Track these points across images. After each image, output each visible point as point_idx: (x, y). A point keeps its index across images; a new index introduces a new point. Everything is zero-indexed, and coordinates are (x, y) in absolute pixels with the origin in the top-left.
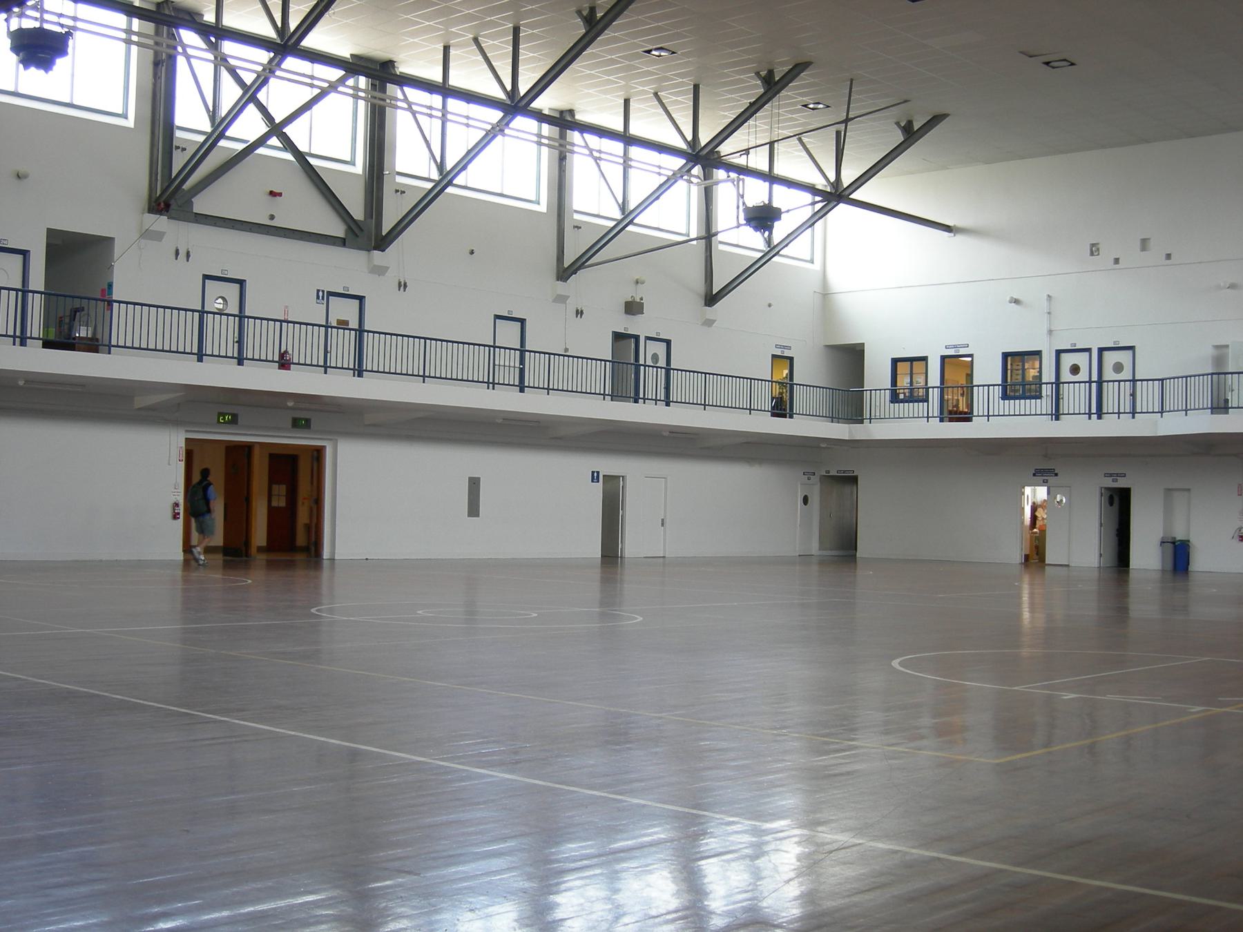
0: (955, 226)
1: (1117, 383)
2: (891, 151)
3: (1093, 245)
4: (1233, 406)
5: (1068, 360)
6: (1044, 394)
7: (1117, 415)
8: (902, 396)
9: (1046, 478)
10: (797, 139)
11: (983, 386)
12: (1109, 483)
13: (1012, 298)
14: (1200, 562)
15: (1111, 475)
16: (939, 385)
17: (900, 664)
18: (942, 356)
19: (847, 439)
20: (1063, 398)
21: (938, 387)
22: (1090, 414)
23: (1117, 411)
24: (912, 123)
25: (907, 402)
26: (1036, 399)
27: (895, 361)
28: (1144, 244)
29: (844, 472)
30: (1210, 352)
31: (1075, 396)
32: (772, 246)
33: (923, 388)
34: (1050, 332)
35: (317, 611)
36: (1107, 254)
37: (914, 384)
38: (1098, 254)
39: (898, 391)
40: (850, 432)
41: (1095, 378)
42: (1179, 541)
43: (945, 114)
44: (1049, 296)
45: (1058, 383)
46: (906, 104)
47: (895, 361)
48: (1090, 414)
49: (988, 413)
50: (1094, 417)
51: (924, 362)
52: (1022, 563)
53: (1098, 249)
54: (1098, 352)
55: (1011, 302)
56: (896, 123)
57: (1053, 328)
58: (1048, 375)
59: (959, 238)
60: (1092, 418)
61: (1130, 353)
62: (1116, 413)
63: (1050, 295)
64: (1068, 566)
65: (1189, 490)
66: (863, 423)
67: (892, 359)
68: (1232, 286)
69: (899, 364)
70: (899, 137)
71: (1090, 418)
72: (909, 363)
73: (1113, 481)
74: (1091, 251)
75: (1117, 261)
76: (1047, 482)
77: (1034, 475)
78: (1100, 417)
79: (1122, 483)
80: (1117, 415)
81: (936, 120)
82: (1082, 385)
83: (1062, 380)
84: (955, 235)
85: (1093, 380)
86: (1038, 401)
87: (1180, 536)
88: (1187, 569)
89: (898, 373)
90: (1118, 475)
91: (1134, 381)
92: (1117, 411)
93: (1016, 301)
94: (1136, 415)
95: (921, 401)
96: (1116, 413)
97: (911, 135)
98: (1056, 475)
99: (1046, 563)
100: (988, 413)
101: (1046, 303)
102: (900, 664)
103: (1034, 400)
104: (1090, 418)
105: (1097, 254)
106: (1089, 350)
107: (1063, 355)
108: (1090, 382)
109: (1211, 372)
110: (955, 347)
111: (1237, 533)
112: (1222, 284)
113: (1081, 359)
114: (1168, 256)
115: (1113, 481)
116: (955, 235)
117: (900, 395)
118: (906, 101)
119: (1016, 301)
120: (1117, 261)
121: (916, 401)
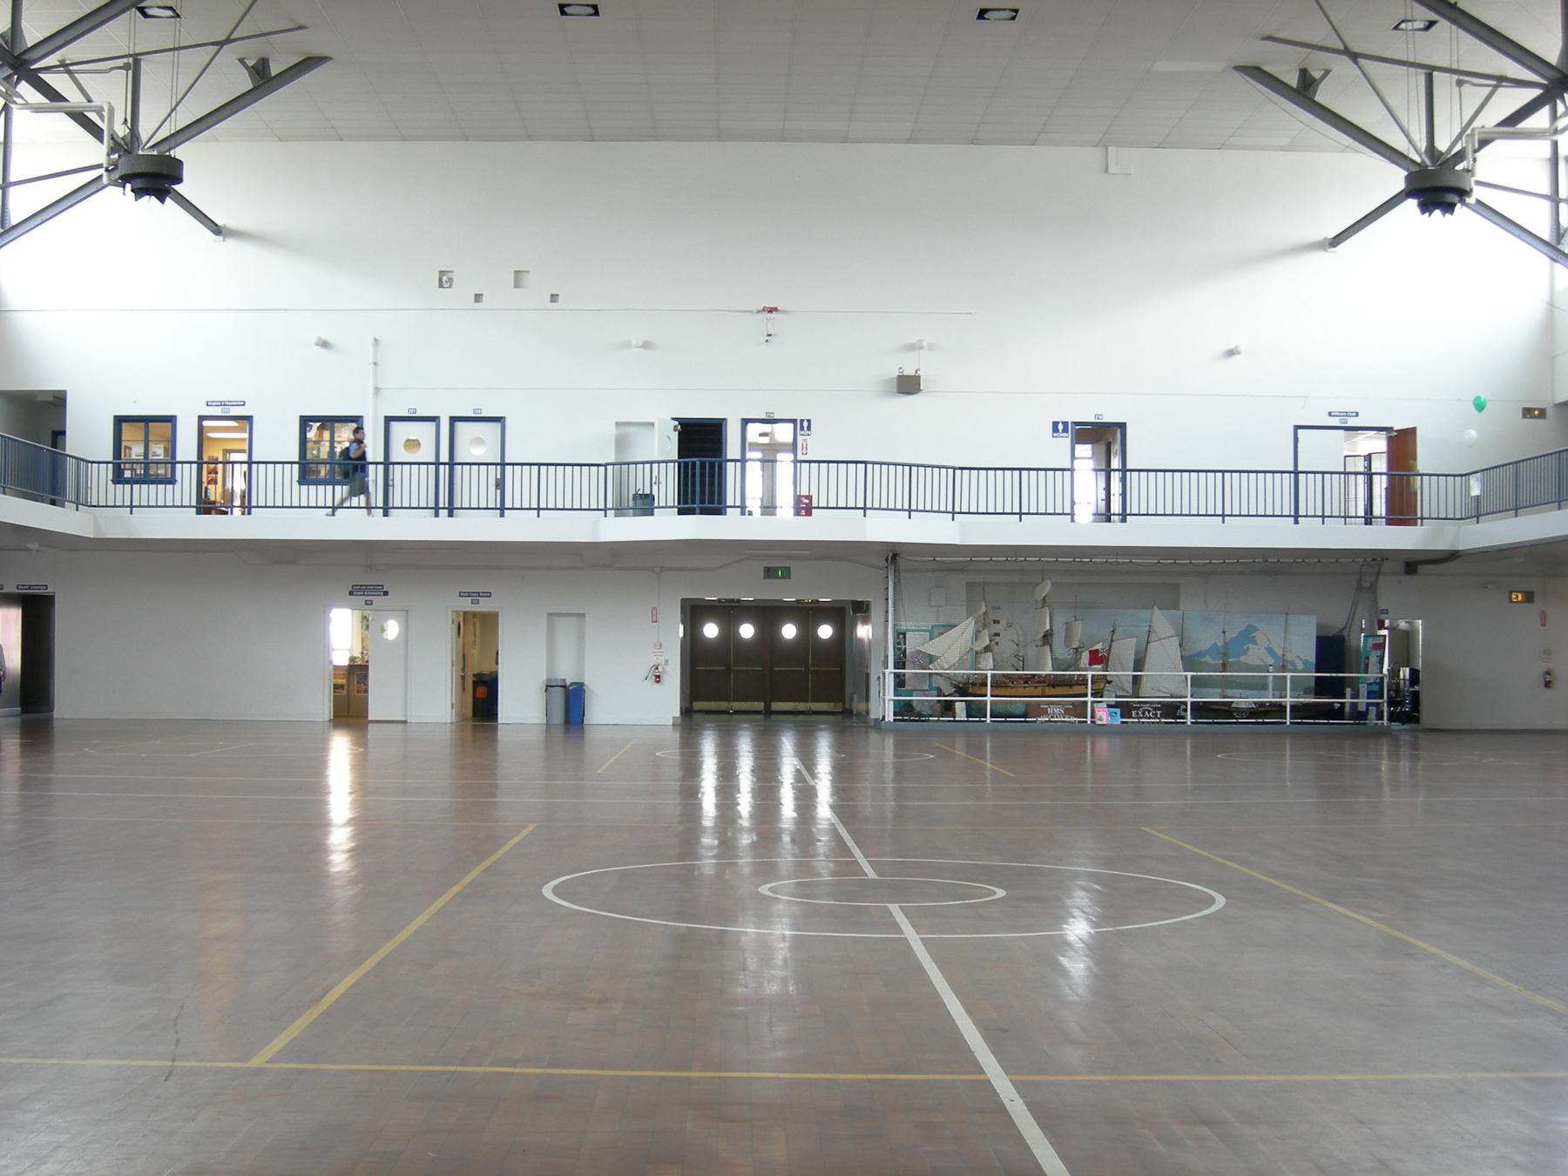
0: (225, 226)
1: (649, 465)
2: (233, 100)
3: (442, 273)
4: (1133, 512)
5: (401, 431)
6: (178, 477)
7: (536, 511)
8: (127, 474)
9: (367, 598)
10: (1426, 74)
11: (644, 463)
12: (466, 605)
13: (320, 338)
14: (598, 712)
15: (469, 595)
16: (111, 459)
17: (1212, 901)
18: (301, 417)
19: (92, 536)
20: (393, 486)
21: (674, 462)
22: (437, 509)
23: (1321, 514)
24: (268, 63)
25: (137, 482)
26: (342, 485)
27: (120, 421)
28: (519, 278)
29: (30, 587)
30: (612, 431)
31: (413, 484)
32: (7, 227)
33: (141, 463)
34: (377, 390)
35: (769, 889)
36: (464, 287)
37: (150, 457)
38: (450, 287)
39: (122, 465)
40: (96, 524)
41: (444, 458)
42: (573, 684)
43: (326, 58)
44: (376, 340)
45: (387, 463)
46: (300, 31)
47: (120, 421)
48: (437, 509)
49: (865, 505)
50: (443, 513)
51: (170, 424)
52: (330, 721)
53: (450, 280)
54: (742, 424)
55: (317, 345)
56: (239, 60)
57: (379, 387)
58: (374, 452)
59: (230, 244)
60: (506, 515)
61: (496, 426)
62: (127, 507)
63: (377, 337)
64: (405, 722)
65: (582, 615)
66: (652, 514)
67: (115, 417)
68: (646, 345)
69: (124, 425)
70: (245, 84)
71: (437, 515)
72: (143, 424)
73: (472, 603)
74: (440, 280)
75: (478, 298)
76: (371, 604)
77: (351, 593)
78: (386, 514)
79: (484, 606)
80: (536, 511)
81: (309, 63)
82: (287, 467)
83: (393, 459)
84: (224, 240)
85: (441, 460)
86: (169, 487)
87: (567, 674)
88: (583, 722)
89: (123, 438)
90: (479, 594)
91: (503, 464)
92: (129, 504)
93: (324, 344)
94: (1299, 519)
95: (161, 482)
96: (127, 507)
97: (264, 79)
98: (386, 593)
99: (370, 718)
100: (865, 505)
101: (371, 348)
102: (556, 891)
103: (315, 487)
104: (437, 515)
105: (447, 286)
106: (796, 420)
107: (394, 425)
108: (437, 464)
109: (613, 461)
110: (222, 404)
111: (1118, 682)
112: (634, 342)
113: (423, 432)
114: (554, 298)
115: (472, 603)
116: (224, 240)
117: (126, 472)
118: (301, 28)
119: (324, 344)
120: (478, 298)
121: (153, 482)
